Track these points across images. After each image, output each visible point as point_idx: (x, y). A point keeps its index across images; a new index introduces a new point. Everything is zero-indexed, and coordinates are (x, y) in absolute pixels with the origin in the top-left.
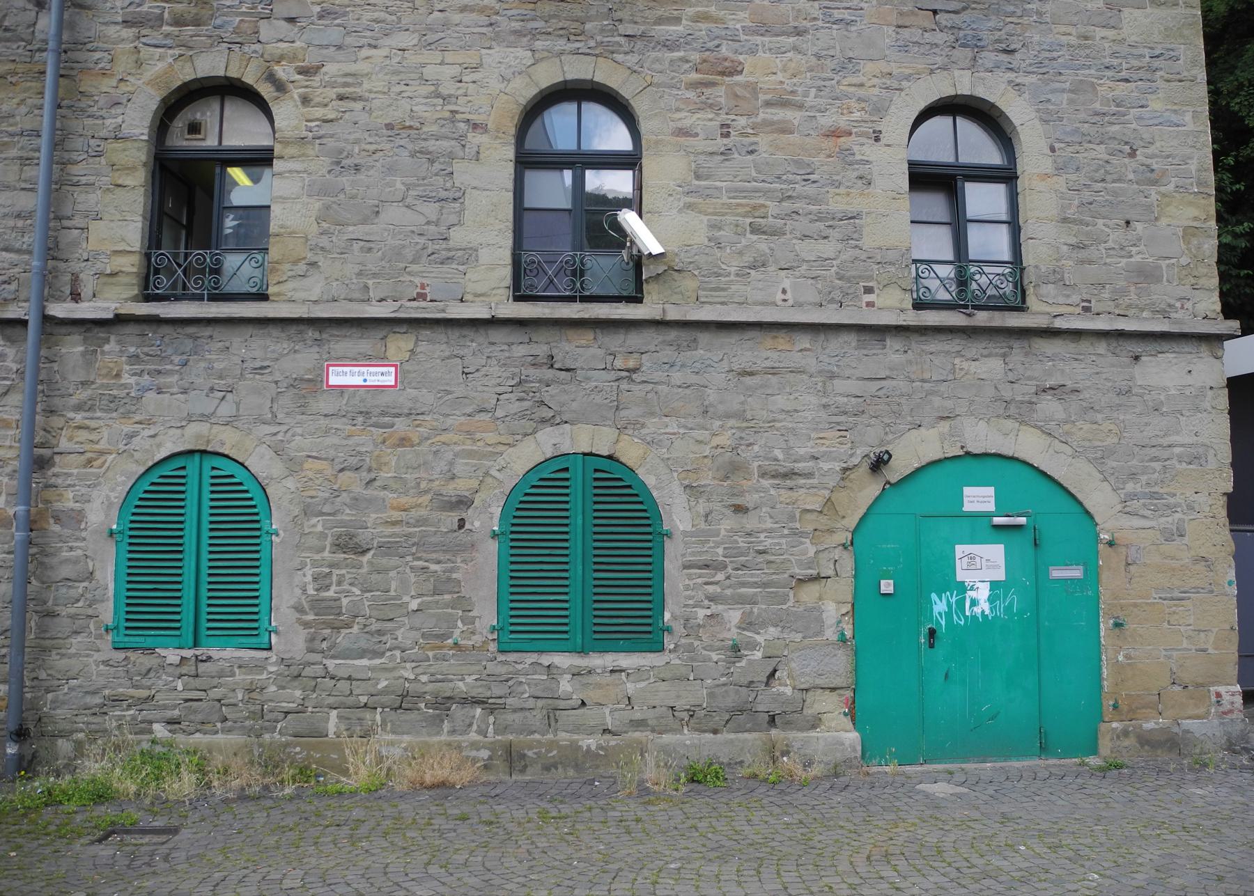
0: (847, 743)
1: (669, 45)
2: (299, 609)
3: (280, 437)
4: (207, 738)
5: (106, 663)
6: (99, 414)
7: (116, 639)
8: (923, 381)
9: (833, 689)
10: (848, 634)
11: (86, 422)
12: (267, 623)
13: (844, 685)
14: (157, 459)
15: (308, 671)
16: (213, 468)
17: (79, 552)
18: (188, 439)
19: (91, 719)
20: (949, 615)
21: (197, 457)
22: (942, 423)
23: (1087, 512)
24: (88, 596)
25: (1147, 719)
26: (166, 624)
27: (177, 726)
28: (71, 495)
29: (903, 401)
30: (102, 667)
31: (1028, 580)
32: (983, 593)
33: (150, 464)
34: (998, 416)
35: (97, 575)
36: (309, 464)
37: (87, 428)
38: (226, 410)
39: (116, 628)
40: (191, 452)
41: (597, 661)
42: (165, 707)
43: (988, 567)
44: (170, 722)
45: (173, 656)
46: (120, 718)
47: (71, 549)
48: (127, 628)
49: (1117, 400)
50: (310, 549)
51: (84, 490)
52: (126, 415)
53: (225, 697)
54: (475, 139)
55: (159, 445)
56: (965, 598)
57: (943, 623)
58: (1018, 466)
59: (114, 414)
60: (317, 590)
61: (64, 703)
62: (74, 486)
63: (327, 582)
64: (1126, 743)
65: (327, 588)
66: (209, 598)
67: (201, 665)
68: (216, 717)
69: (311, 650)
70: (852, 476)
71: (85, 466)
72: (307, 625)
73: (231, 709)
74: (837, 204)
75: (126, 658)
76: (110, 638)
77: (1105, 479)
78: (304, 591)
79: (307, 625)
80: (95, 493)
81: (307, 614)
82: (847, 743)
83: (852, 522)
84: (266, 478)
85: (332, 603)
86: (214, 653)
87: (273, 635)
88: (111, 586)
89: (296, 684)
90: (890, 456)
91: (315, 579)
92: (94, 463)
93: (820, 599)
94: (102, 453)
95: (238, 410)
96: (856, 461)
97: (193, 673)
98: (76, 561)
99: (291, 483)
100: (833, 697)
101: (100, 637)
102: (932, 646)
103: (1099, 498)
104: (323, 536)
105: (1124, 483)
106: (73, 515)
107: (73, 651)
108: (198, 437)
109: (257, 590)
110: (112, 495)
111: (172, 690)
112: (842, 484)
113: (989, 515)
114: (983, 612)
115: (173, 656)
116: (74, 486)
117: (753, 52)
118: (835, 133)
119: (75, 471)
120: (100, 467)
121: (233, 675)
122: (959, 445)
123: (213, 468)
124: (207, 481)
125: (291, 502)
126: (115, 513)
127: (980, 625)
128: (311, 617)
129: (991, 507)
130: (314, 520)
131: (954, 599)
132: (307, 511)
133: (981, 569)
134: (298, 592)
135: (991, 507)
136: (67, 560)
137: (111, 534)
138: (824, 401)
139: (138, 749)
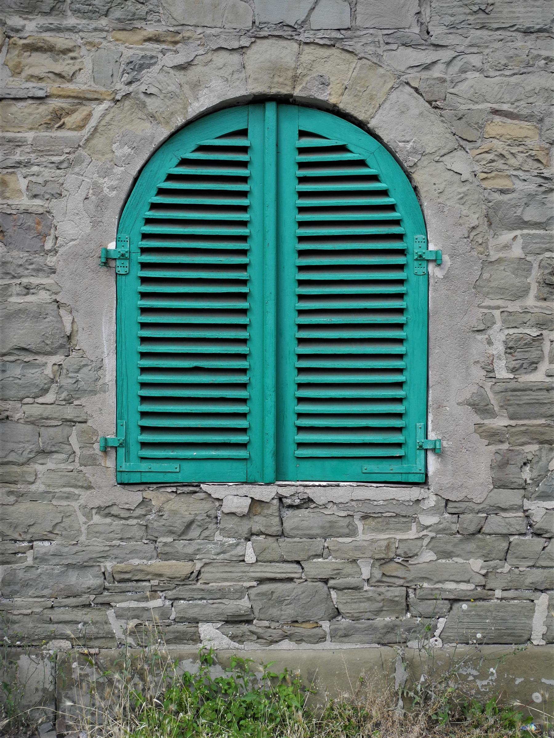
2: (481, 408)
3: (437, 72)
4: (306, 651)
5: (104, 510)
6: (71, 21)
7: (125, 467)
11: (47, 36)
12: (421, 433)
14: (197, 107)
15: (495, 523)
16: (303, 134)
17: (44, 296)
18: (259, 69)
19: (79, 615)
21: (271, 109)
24: (66, 382)
26: (225, 439)
27: (245, 628)
28: (23, 184)
30: (97, 519)
33: (180, 121)
35: (82, 340)
36: (497, 126)
37: (49, 49)
39: (124, 444)
40: (258, 101)
42: (222, 594)
44: (233, 620)
45: (235, 499)
46: (136, 614)
47: (28, 289)
48: (144, 445)
50: (501, 291)
51: (48, 173)
52: (127, 25)
53: (338, 573)
55: (196, 86)
59: (103, 22)
60: (513, 370)
61: (26, 585)
62: (28, 164)
63: (533, 355)
65: (533, 365)
66: (301, 386)
67: (288, 514)
68: (320, 610)
69: (500, 485)
71: (48, 126)
72: (494, 436)
73: (348, 595)
75: (144, 502)
76: (110, 463)
78: (490, 371)
79: (494, 436)
80: (71, 180)
81: (492, 414)
84: (414, 151)
85: (542, 396)
86: (319, 495)
87: (431, 458)
88: (110, 363)
89: (471, 546)
91: (510, 349)
92: (69, 120)
94: (82, 99)
95: (353, 15)
97: (276, 529)
98: (39, 315)
99: (460, 163)
101: (92, 461)
104: (522, 266)
106: (30, 221)
107: (39, 487)
108: (275, 69)
109: (400, 371)
110: (106, 183)
111: (235, 562)
115: (235, 499)
116: (28, 164)
119: (30, 136)
120: (81, 127)
121: (352, 533)
123: (303, 134)
124: (291, 158)
125: (462, 200)
126: (111, 217)
128: (500, 422)
130: (506, 237)
132: (494, 219)
134: (478, 374)
136: (20, 313)
137: (107, 261)
139: (176, 673)
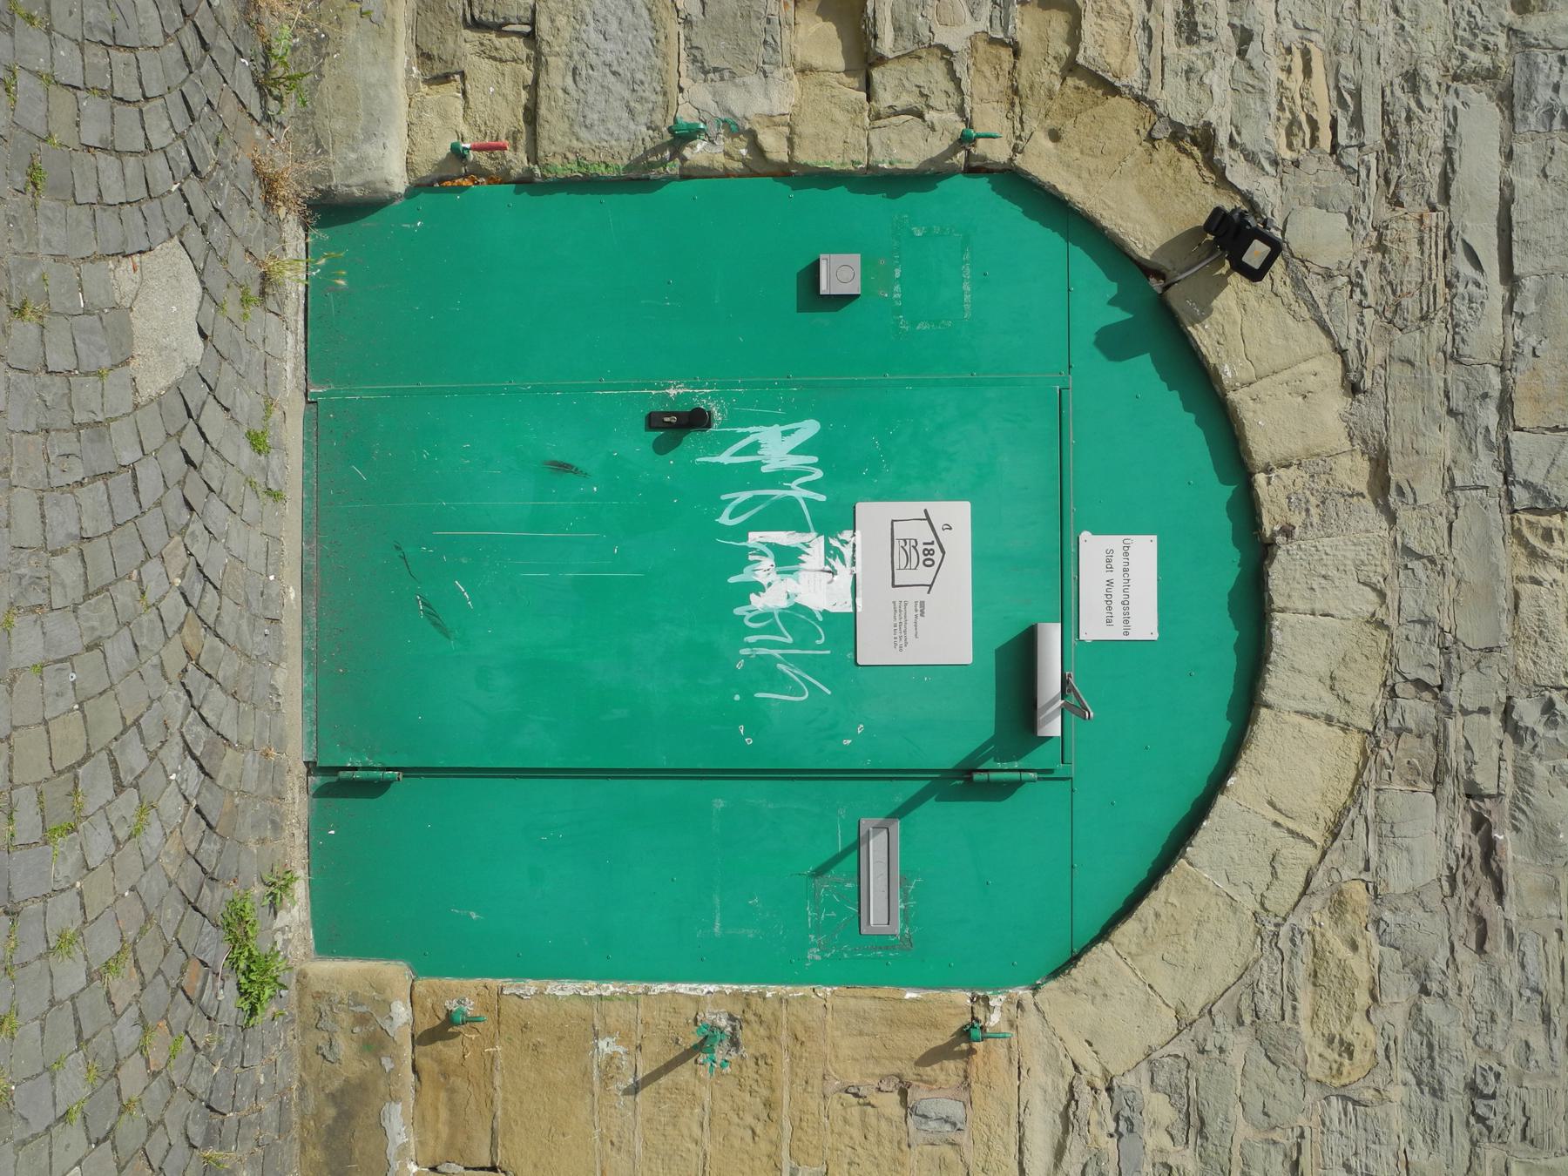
0: (370, 150)
8: (1506, 404)
9: (531, 115)
10: (698, 152)
13: (544, 144)
20: (751, 475)
22: (1364, 466)
23: (1074, 960)
25: (419, 1121)
29: (1438, 333)
32: (817, 588)
34: (1391, 657)
43: (899, 608)
49: (1454, 1079)
56: (802, 528)
57: (725, 458)
58: (1226, 664)
64: (345, 1047)
70: (1187, 163)
77: (1184, 1025)
82: (370, 150)
83: (1042, 162)
90: (1255, 275)
93: (805, 70)
96: (1239, 174)
100: (509, 118)
102: (653, 421)
105: (1171, 1092)
112: (1162, 132)
113: (1068, 613)
114: (758, 588)
122: (1297, 519)
127: (716, 574)
129: (1093, 628)
131: (799, 494)
135: (1093, 628)
138: (1432, 74)
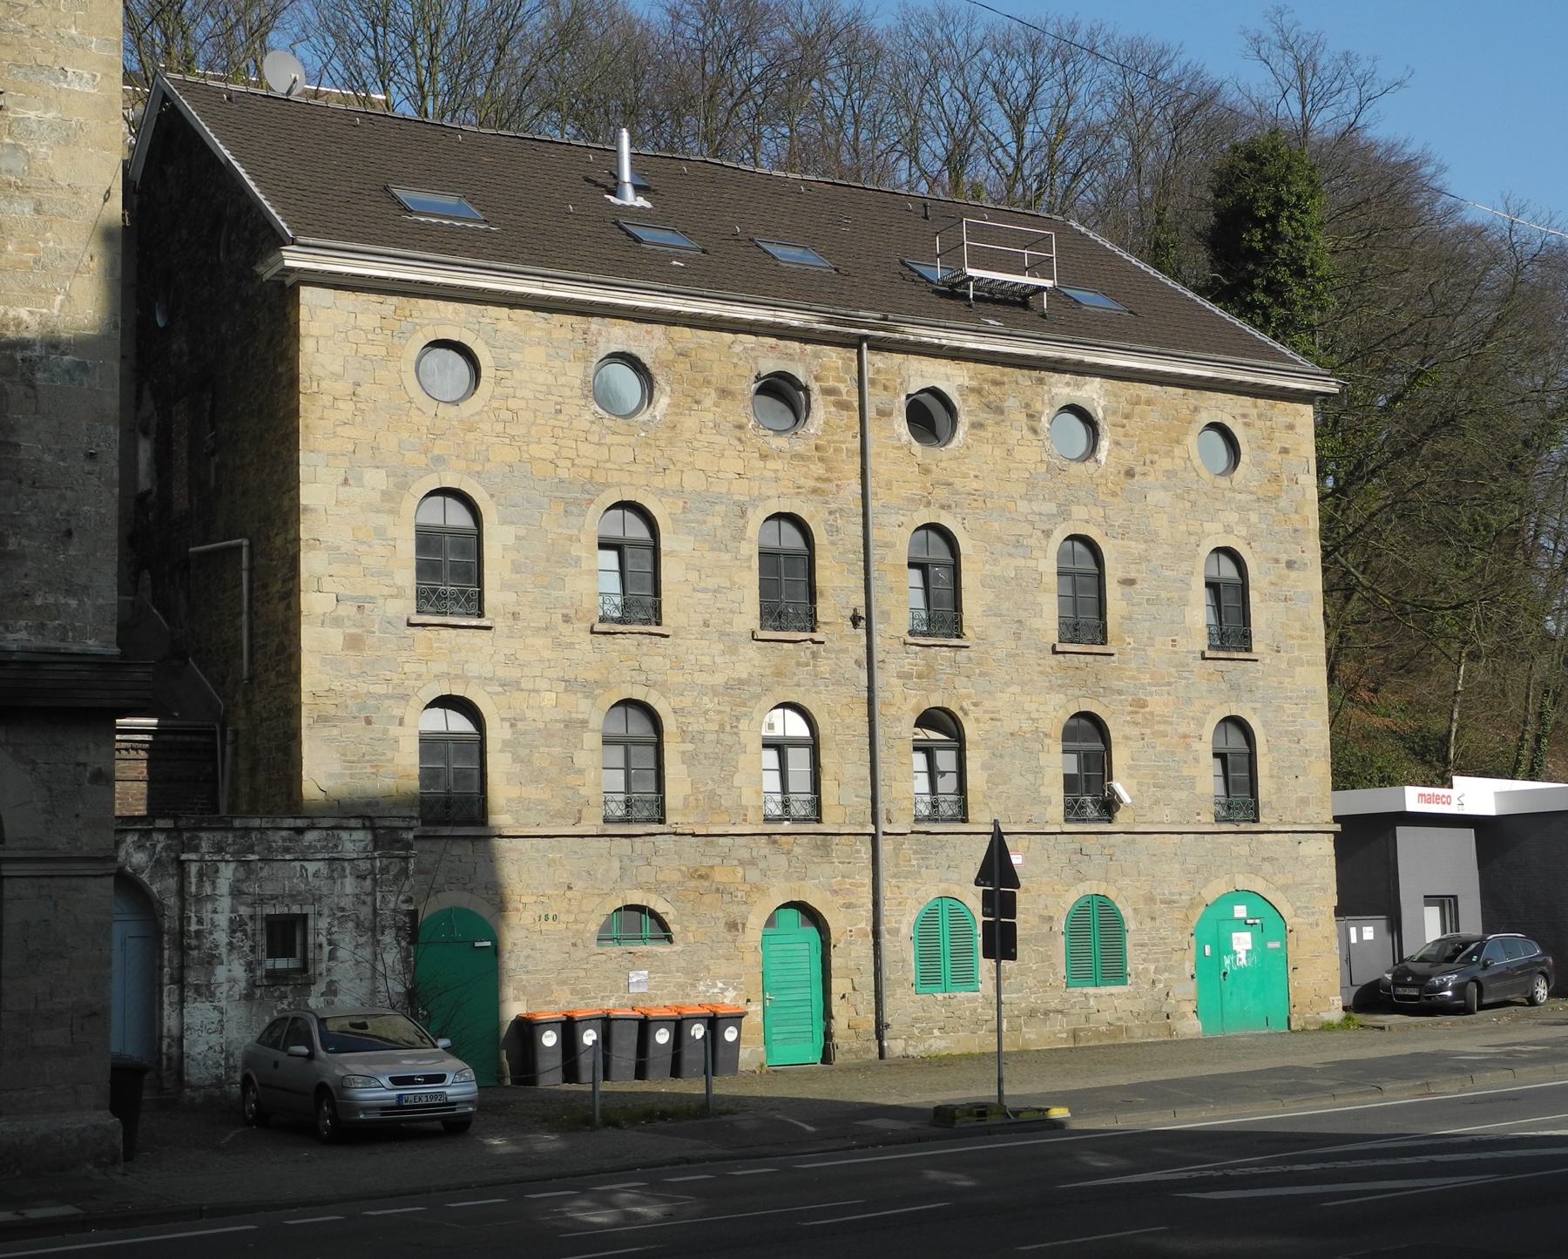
1: (1120, 692)
31: (1258, 950)
32: (1243, 955)
38: (955, 876)
41: (1104, 990)
45: (940, 997)
54: (1047, 741)
74: (1185, 772)
103: (1286, 910)
117: (1151, 694)
118: (1185, 736)
127: (1243, 970)
133: (1242, 942)
